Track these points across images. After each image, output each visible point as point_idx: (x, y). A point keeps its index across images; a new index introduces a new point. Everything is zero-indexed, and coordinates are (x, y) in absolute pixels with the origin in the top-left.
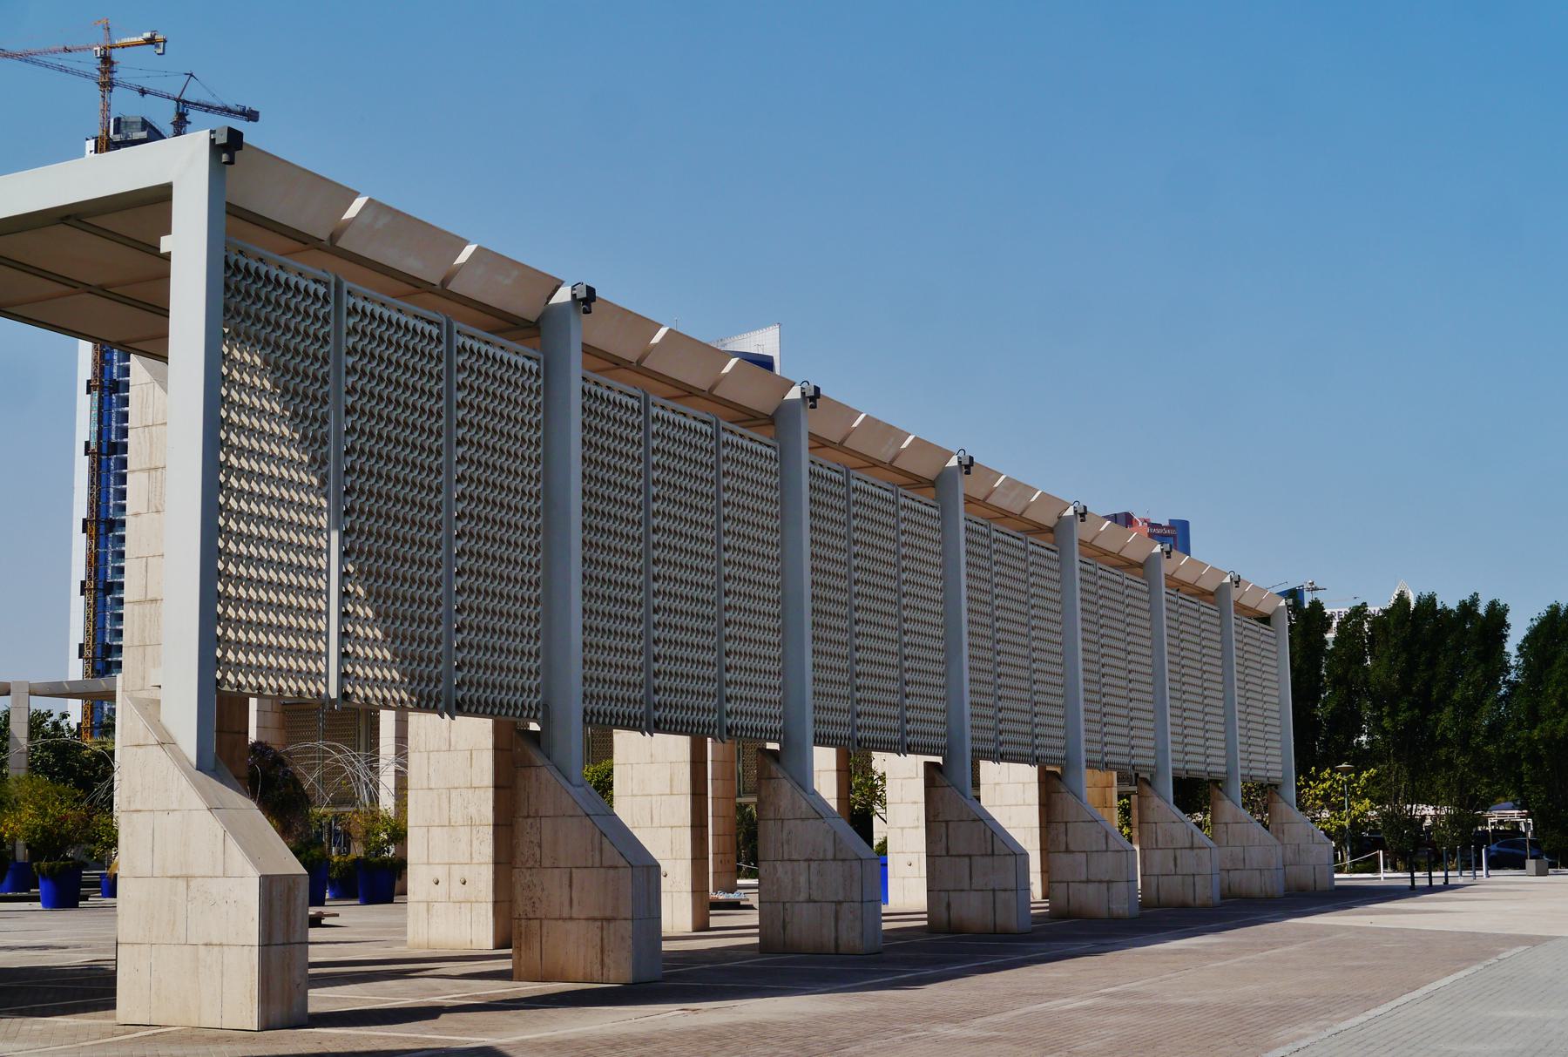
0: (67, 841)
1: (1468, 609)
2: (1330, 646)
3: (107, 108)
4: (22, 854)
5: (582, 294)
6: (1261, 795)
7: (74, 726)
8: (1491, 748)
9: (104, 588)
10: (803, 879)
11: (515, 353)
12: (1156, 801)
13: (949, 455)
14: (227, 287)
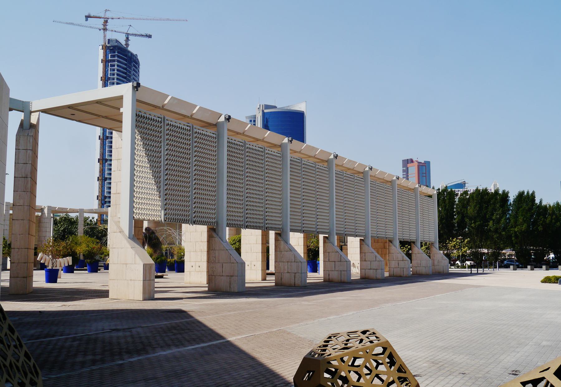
0: (95, 254)
1: (497, 192)
2: (457, 202)
3: (105, 36)
4: (82, 258)
5: (227, 117)
6: (428, 247)
7: (95, 221)
8: (504, 233)
9: (105, 179)
10: (286, 267)
11: (209, 132)
12: (393, 247)
13: (331, 154)
14: (136, 120)
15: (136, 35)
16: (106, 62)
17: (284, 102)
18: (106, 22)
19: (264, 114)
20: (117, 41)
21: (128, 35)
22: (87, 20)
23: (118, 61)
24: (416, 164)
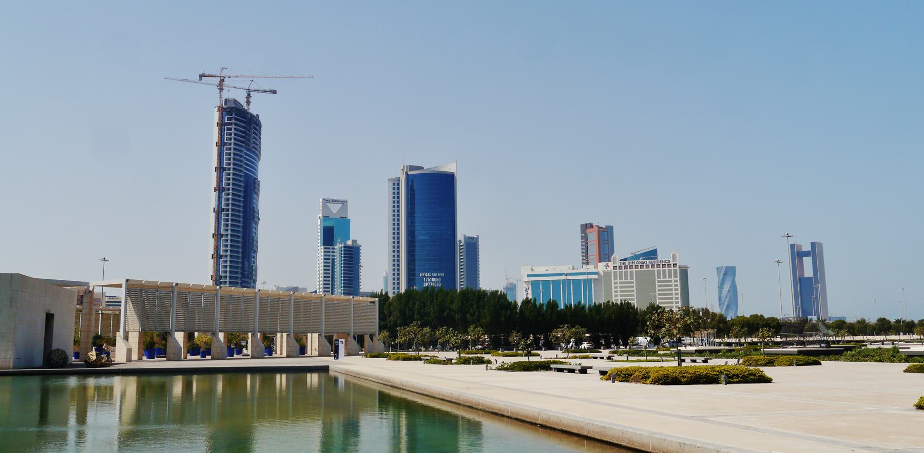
15: (258, 91)
16: (221, 125)
17: (433, 162)
18: (222, 81)
19: (407, 176)
20: (235, 101)
21: (249, 90)
22: (201, 79)
23: (236, 124)
24: (596, 229)
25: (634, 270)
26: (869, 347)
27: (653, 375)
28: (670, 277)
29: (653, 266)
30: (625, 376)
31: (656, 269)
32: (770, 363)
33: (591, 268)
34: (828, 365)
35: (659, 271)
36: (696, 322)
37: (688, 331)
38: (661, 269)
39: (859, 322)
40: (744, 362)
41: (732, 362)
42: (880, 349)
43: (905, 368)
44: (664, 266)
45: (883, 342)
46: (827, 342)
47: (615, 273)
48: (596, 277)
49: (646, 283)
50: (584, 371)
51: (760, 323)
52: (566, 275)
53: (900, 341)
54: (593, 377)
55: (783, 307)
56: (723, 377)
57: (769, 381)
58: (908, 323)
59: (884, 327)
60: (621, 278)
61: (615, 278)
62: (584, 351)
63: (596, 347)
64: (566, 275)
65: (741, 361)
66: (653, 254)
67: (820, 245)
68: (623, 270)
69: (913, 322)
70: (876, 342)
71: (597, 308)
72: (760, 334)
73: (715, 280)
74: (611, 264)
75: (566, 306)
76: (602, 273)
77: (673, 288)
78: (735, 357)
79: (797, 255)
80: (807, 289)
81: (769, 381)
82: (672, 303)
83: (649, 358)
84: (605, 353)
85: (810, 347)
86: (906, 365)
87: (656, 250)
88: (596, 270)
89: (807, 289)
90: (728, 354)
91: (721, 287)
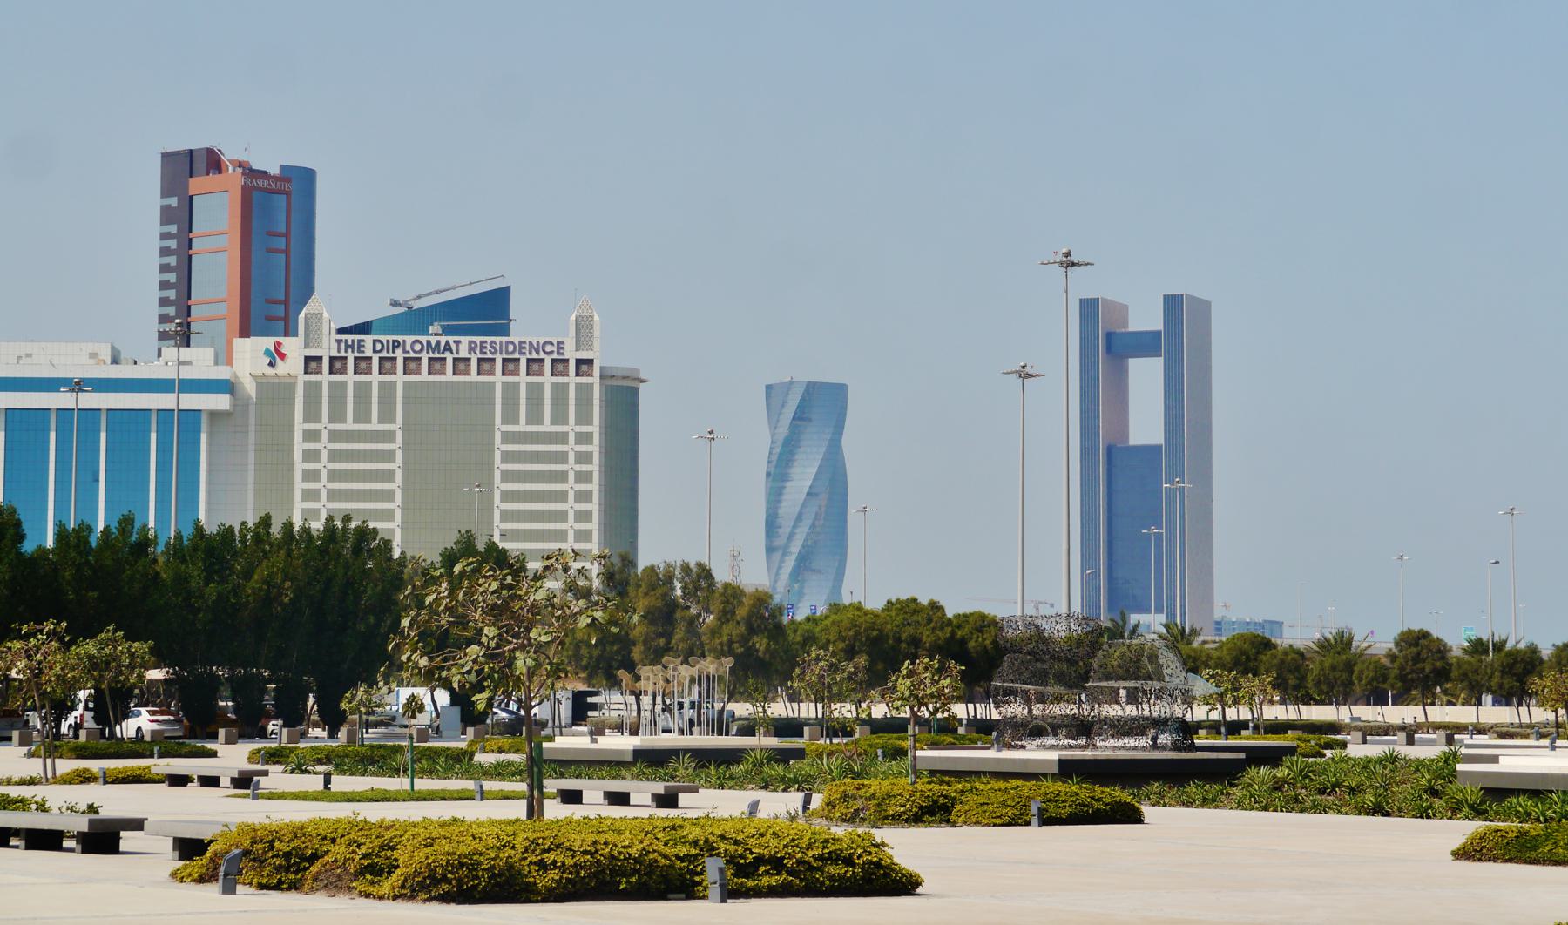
24: (234, 178)
25: (400, 378)
26: (1356, 750)
27: (409, 859)
28: (559, 417)
29: (485, 364)
30: (285, 863)
31: (498, 379)
32: (936, 812)
33: (199, 361)
34: (1169, 823)
35: (511, 391)
36: (644, 620)
37: (610, 660)
38: (523, 379)
39: (1324, 645)
40: (830, 804)
41: (778, 805)
42: (1394, 759)
43: (1458, 841)
44: (534, 365)
45: (1410, 733)
46: (1187, 729)
47: (312, 391)
48: (221, 402)
49: (448, 446)
50: (102, 838)
51: (927, 638)
52: (78, 386)
53: (1480, 730)
54: (147, 861)
55: (1032, 580)
56: (712, 868)
57: (905, 885)
58: (1515, 655)
59: (1421, 669)
60: (337, 415)
61: (312, 414)
62: (138, 747)
63: (197, 723)
64: (78, 386)
65: (817, 801)
66: (487, 310)
67: (1203, 308)
68: (350, 377)
69: (1533, 650)
70: (1387, 730)
71: (212, 551)
72: (904, 685)
73: (754, 440)
74: (294, 347)
75: (61, 534)
76: (250, 388)
77: (571, 467)
78: (805, 784)
79: (1107, 345)
80: (1137, 499)
81: (905, 885)
82: (553, 528)
83: (423, 784)
84: (232, 756)
85: (1107, 748)
86: (1464, 830)
87: (505, 292)
88: (222, 373)
89: (1137, 499)
90: (778, 769)
91: (778, 474)
